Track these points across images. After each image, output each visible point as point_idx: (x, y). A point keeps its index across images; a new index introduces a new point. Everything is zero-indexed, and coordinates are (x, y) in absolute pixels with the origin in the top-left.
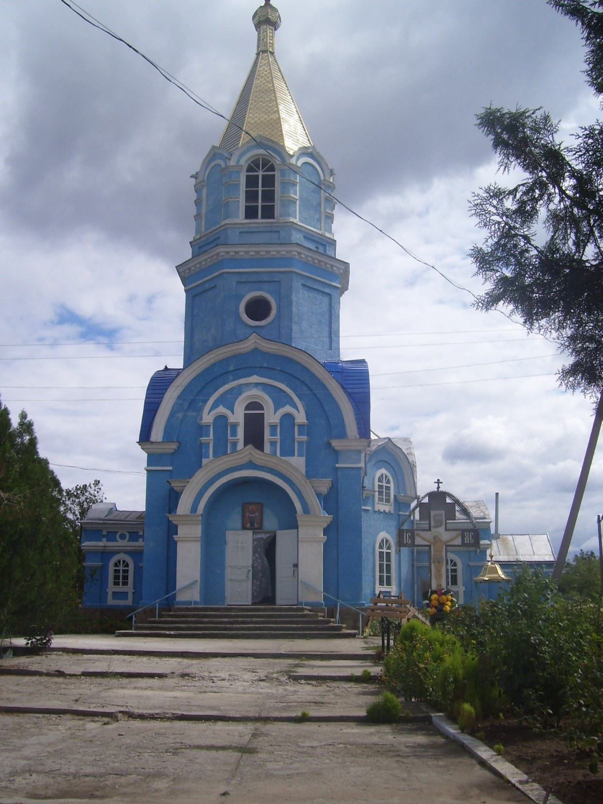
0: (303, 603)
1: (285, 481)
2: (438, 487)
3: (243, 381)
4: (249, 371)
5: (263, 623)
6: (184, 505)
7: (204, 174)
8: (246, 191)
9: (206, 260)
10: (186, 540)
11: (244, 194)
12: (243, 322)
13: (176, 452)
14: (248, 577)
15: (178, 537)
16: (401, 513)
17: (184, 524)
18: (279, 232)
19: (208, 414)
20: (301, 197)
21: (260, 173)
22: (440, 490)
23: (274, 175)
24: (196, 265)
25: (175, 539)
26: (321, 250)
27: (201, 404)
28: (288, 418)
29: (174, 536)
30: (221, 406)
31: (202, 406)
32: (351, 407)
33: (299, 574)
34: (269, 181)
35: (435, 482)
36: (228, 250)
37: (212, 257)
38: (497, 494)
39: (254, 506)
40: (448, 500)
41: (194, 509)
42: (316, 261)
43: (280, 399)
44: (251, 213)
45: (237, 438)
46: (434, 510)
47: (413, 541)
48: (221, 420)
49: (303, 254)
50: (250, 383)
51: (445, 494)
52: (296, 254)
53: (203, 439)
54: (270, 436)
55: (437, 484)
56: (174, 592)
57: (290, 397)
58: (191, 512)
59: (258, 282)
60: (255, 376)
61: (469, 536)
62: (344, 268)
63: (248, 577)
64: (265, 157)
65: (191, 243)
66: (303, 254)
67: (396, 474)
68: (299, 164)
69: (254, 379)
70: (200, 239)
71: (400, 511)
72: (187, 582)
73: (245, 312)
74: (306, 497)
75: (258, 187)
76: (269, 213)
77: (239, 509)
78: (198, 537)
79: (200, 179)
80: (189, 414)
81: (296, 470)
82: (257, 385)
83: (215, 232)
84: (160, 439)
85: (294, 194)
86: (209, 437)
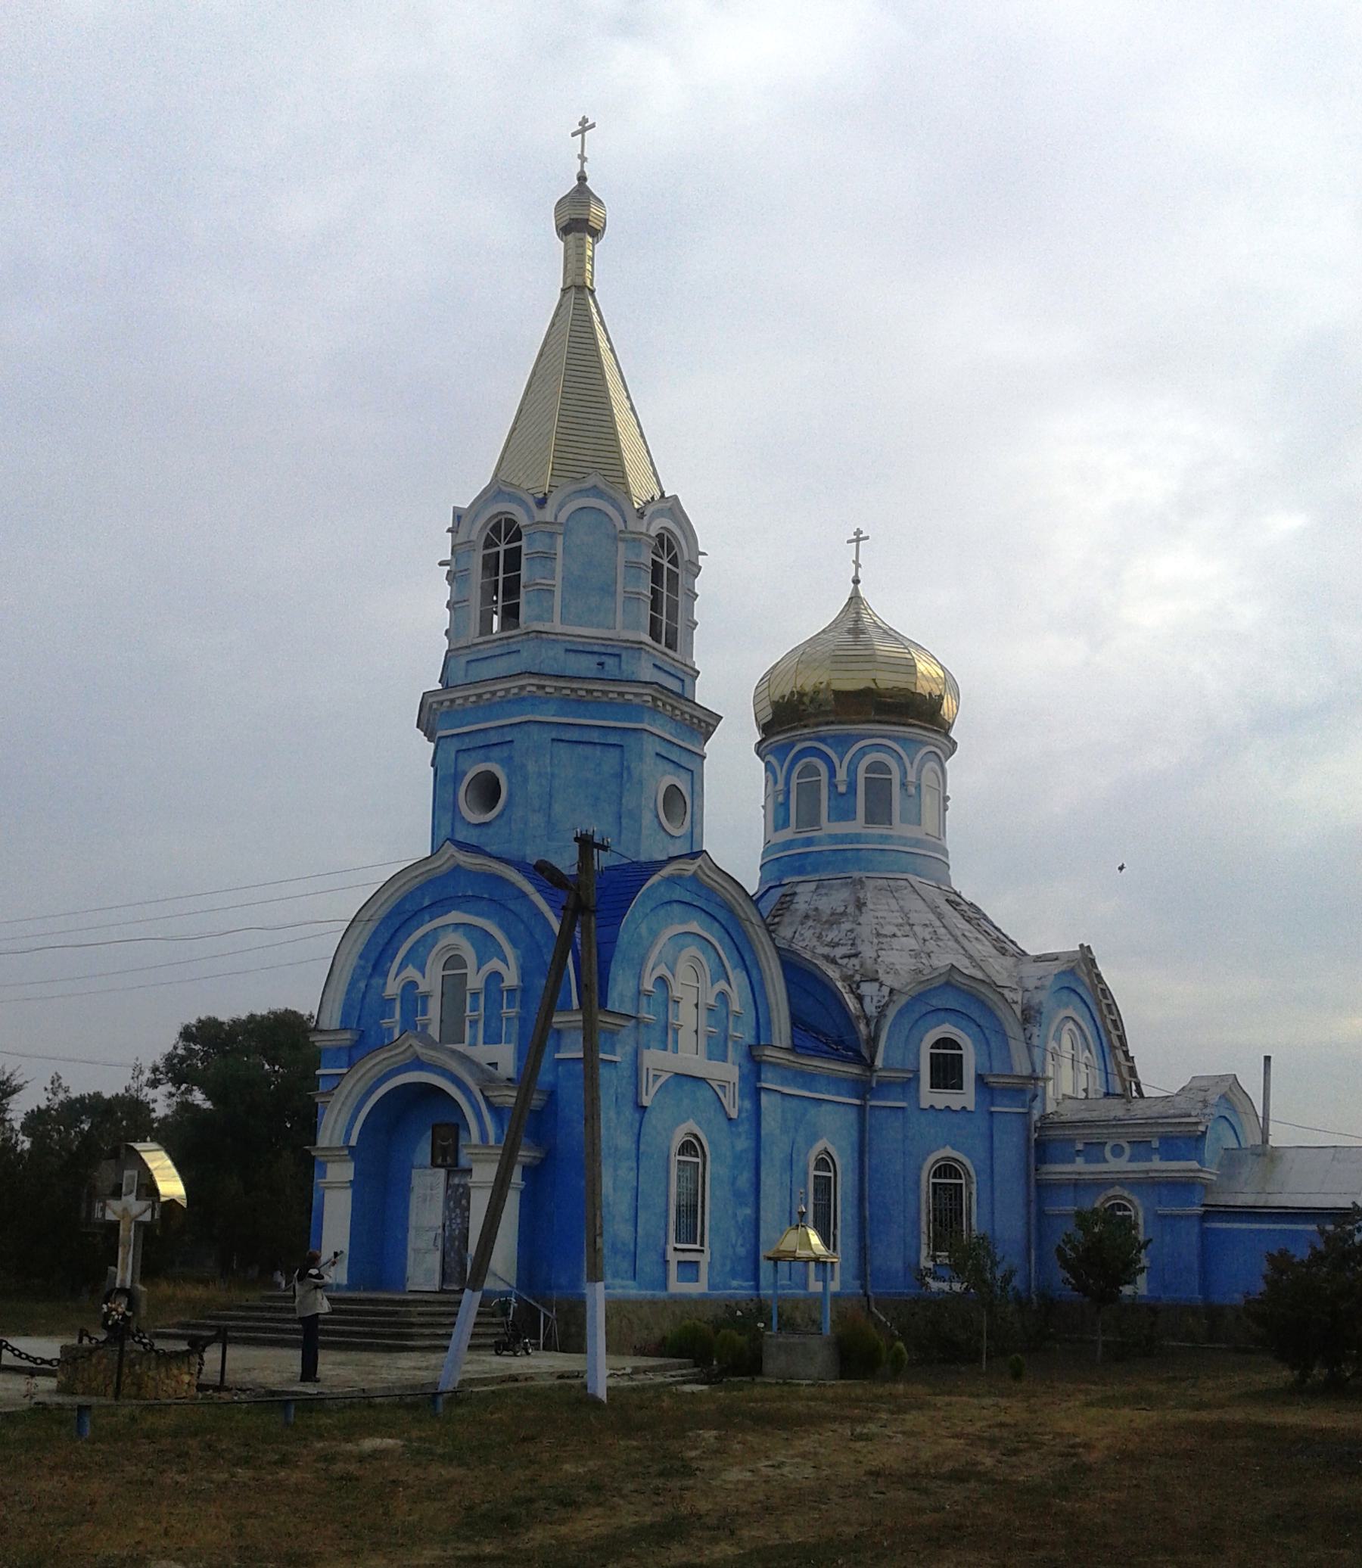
4: (440, 906)
10: (331, 1186)
19: (478, 972)
28: (496, 976)
30: (495, 959)
38: (1267, 1059)
43: (485, 944)
50: (448, 925)
53: (386, 1022)
69: (455, 916)
71: (993, 1104)
82: (457, 925)
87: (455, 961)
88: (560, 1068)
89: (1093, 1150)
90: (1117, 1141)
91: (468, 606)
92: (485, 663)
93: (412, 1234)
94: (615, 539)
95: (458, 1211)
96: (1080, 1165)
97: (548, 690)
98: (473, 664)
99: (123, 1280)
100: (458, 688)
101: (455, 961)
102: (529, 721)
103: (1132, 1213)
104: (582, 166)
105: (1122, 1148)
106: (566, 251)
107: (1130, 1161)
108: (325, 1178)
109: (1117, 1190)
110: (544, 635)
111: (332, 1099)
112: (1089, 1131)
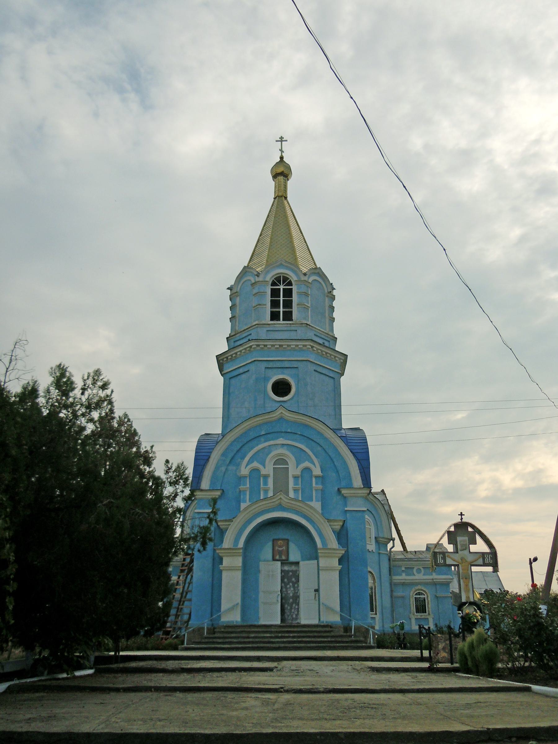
2: (462, 519)
3: (272, 442)
9: (240, 351)
10: (230, 569)
19: (245, 468)
20: (311, 305)
21: (282, 287)
22: (463, 520)
23: (292, 289)
24: (233, 354)
34: (288, 293)
35: (459, 515)
37: (245, 349)
41: (237, 540)
42: (324, 353)
43: (300, 456)
44: (275, 316)
45: (268, 487)
46: (460, 536)
47: (445, 561)
49: (315, 347)
51: (468, 524)
54: (294, 485)
56: (220, 613)
57: (309, 455)
61: (488, 558)
63: (277, 601)
66: (315, 347)
67: (375, 520)
68: (310, 281)
69: (281, 441)
75: (283, 300)
76: (288, 316)
77: (270, 544)
78: (240, 567)
80: (230, 468)
84: (207, 488)
88: (348, 515)
90: (418, 567)
91: (266, 307)
92: (276, 333)
93: (261, 595)
95: (291, 584)
98: (270, 332)
99: (468, 597)
103: (426, 596)
106: (275, 184)
107: (424, 575)
109: (419, 587)
110: (309, 326)
111: (232, 524)
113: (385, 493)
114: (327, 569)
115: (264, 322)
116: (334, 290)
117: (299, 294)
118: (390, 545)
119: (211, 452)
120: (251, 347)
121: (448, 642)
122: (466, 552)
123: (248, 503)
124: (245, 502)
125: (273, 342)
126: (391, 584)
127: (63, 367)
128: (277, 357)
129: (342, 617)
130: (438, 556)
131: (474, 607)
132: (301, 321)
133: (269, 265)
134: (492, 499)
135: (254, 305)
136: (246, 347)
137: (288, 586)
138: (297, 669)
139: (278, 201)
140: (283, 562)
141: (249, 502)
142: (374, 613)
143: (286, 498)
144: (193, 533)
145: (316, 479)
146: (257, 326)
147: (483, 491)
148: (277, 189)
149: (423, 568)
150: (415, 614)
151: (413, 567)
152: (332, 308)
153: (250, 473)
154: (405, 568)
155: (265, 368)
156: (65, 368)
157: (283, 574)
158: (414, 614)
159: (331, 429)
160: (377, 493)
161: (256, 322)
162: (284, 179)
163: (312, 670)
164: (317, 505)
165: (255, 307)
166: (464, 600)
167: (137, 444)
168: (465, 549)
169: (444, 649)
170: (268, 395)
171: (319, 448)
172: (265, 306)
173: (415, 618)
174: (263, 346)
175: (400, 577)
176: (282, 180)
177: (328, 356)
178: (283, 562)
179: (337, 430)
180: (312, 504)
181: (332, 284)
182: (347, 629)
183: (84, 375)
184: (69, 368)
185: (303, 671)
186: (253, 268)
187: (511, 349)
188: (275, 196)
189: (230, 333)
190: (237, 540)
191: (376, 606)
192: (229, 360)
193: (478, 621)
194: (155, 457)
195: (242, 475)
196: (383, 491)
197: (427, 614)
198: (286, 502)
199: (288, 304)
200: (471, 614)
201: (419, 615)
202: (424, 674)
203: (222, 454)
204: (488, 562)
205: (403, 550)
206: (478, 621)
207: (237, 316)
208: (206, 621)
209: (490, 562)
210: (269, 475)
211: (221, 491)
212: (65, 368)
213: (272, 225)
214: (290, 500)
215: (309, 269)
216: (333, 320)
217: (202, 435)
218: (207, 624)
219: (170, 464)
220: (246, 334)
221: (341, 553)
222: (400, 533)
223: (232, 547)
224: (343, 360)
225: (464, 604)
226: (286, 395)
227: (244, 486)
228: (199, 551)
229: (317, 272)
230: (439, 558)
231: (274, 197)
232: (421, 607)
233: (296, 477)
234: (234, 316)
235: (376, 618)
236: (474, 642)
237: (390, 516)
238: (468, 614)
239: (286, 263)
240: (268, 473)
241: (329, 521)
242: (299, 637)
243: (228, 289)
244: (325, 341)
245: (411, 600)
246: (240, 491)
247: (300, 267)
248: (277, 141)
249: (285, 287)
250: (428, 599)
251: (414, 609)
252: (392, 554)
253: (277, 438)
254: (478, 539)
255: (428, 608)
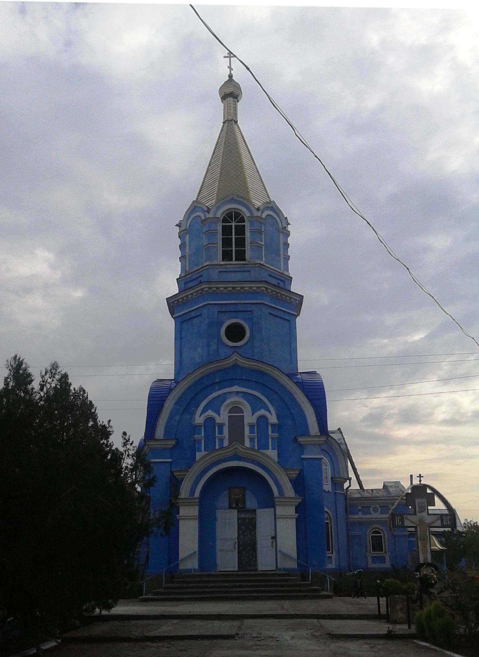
0: (282, 570)
1: (264, 470)
2: (420, 481)
4: (231, 382)
5: (256, 586)
6: (184, 492)
7: (187, 224)
8: (223, 238)
9: (192, 294)
10: (185, 518)
11: (221, 240)
12: (223, 343)
13: (174, 447)
14: (235, 548)
15: (179, 516)
16: (337, 492)
17: (184, 506)
18: (249, 271)
19: (200, 417)
21: (233, 224)
25: (178, 518)
26: (281, 284)
27: (193, 409)
29: (177, 515)
31: (194, 410)
32: (313, 411)
33: (278, 545)
34: (241, 230)
35: (418, 477)
36: (210, 286)
39: (238, 490)
40: (429, 491)
41: (192, 492)
42: (279, 295)
44: (227, 256)
48: (210, 420)
51: (426, 486)
52: (264, 289)
53: (196, 436)
54: (250, 434)
55: (419, 478)
57: (264, 403)
58: (190, 496)
59: (236, 312)
60: (236, 386)
61: (447, 520)
62: (299, 299)
63: (235, 548)
64: (236, 210)
65: (177, 279)
68: (263, 216)
70: (185, 276)
72: (187, 554)
73: (225, 335)
74: (281, 482)
75: (235, 238)
76: (241, 256)
77: (226, 492)
78: (196, 516)
79: (183, 228)
81: (271, 459)
82: (238, 393)
83: (198, 271)
84: (162, 437)
85: (260, 241)
86: (201, 435)
87: (236, 409)
89: (366, 510)
91: (217, 246)
93: (218, 542)
94: (279, 231)
95: (248, 531)
96: (360, 515)
97: (221, 289)
99: (426, 559)
100: (237, 283)
101: (236, 409)
102: (262, 303)
103: (382, 535)
104: (230, 71)
105: (378, 509)
106: (224, 107)
107: (381, 514)
108: (179, 514)
110: (263, 266)
112: (366, 502)
113: (342, 431)
114: (285, 517)
115: (215, 262)
116: (289, 226)
117: (252, 232)
118: (346, 485)
119: (165, 400)
120: (202, 289)
121: (405, 603)
122: (424, 514)
123: (203, 453)
124: (201, 451)
125: (225, 284)
126: (347, 523)
127: (19, 359)
128: (230, 300)
129: (299, 564)
130: (396, 517)
131: (433, 568)
132: (254, 261)
133: (220, 202)
134: (452, 422)
135: (204, 244)
136: (197, 289)
137: (246, 534)
138: (258, 636)
139: (228, 126)
140: (240, 509)
141: (204, 450)
142: (330, 552)
143: (243, 448)
144: (155, 518)
145: (271, 427)
146: (208, 267)
147: (441, 414)
148: (226, 112)
149: (380, 506)
150: (372, 552)
151: (370, 506)
152: (287, 245)
153: (204, 422)
154: (362, 507)
155: (218, 311)
156: (21, 359)
157: (240, 521)
158: (370, 552)
159: (285, 374)
160: (333, 432)
161: (208, 263)
162: (234, 101)
163: (273, 637)
164: (272, 453)
165: (206, 246)
166: (421, 561)
167: (94, 417)
168: (424, 511)
169: (401, 609)
170: (221, 340)
171: (275, 396)
172: (216, 245)
173: (372, 557)
174: (215, 289)
175: (356, 516)
176: (232, 102)
177: (283, 298)
178: (240, 509)
179: (292, 375)
180: (267, 452)
181: (287, 217)
182: (304, 576)
183: (41, 371)
184: (25, 360)
185: (263, 638)
186: (202, 202)
187: (473, 338)
188: (224, 120)
189: (180, 273)
190: (192, 492)
191: (332, 545)
192: (180, 303)
193: (435, 582)
194: (113, 431)
195: (196, 424)
196: (339, 429)
197: (384, 552)
198: (242, 451)
199: (241, 242)
200: (428, 576)
201: (377, 554)
202: (381, 642)
203: (175, 403)
204: (446, 524)
205: (359, 488)
206: (435, 582)
207: (187, 255)
208: (164, 570)
209: (448, 523)
210: (225, 423)
211: (176, 441)
212: (21, 359)
213: (221, 154)
214: (245, 449)
215: (263, 202)
216: (287, 258)
217: (154, 382)
218: (165, 573)
219: (128, 437)
220: (197, 276)
221: (298, 502)
222: (357, 472)
223: (188, 497)
224: (299, 301)
225: (422, 565)
226: (240, 340)
227: (199, 435)
228: (161, 535)
229: (271, 206)
230: (397, 520)
231: (223, 121)
232: (377, 544)
233: (251, 426)
234: (183, 255)
235: (332, 558)
236: (432, 613)
237: (346, 455)
238: (425, 576)
239: (237, 197)
240: (223, 422)
241: (286, 470)
242: (256, 586)
243: (177, 225)
244: (279, 282)
245: (368, 538)
246: (195, 440)
247: (253, 201)
248: (225, 57)
249: (237, 224)
250: (384, 538)
251: (370, 547)
252: (349, 492)
253: (231, 386)
254: (436, 499)
255: (385, 546)
